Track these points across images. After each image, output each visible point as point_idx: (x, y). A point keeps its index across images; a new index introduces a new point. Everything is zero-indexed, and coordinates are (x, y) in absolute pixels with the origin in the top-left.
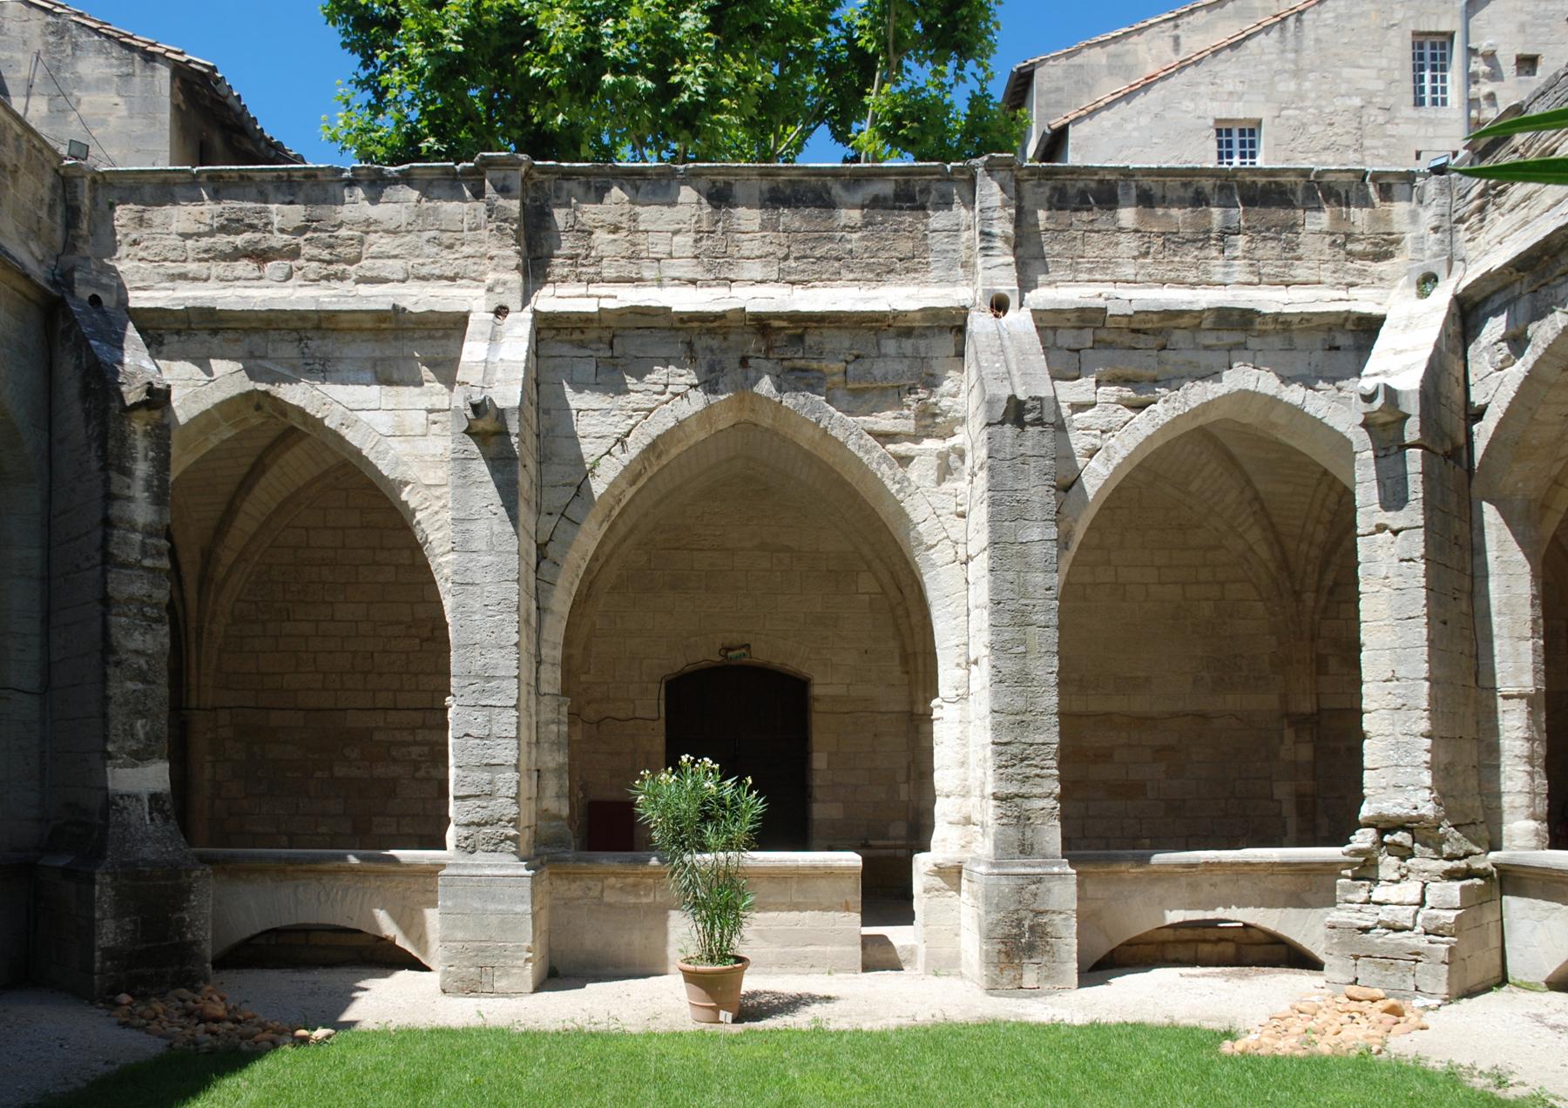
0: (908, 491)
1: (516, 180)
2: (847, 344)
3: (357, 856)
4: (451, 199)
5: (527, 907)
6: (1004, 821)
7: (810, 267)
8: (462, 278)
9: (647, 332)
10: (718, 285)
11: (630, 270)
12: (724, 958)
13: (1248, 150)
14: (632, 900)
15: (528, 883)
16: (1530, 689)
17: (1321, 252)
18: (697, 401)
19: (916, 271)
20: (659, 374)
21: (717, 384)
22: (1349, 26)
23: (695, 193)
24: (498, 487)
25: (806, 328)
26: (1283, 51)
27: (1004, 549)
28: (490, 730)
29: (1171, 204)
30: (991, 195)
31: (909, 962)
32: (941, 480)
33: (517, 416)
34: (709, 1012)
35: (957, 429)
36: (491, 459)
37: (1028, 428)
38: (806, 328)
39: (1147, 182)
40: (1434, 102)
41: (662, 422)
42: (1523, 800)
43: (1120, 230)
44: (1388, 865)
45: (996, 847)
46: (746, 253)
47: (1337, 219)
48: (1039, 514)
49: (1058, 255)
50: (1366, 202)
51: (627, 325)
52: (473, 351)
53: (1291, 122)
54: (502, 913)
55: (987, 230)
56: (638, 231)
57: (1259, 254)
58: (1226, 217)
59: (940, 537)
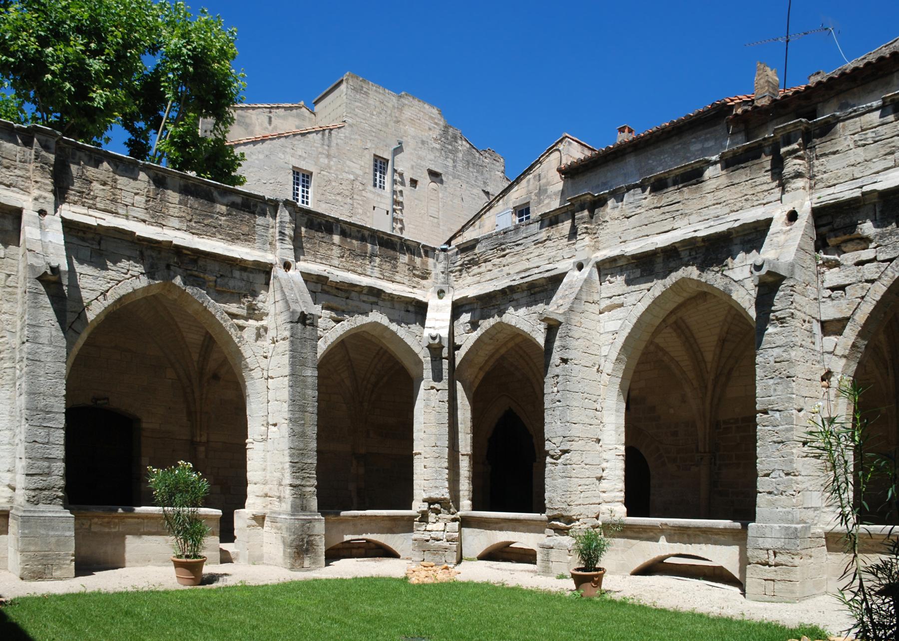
0: (243, 342)
1: (52, 143)
2: (217, 269)
3: (123, 509)
4: (10, 141)
5: (73, 533)
7: (201, 228)
8: (14, 187)
9: (119, 241)
10: (157, 226)
12: (196, 556)
13: (306, 184)
14: (107, 530)
15: (73, 520)
16: (470, 453)
17: (405, 272)
18: (144, 282)
19: (249, 241)
20: (124, 264)
23: (147, 177)
24: (55, 311)
25: (199, 257)
29: (353, 238)
31: (235, 559)
32: (257, 340)
33: (67, 276)
35: (264, 318)
39: (344, 226)
40: (380, 187)
41: (125, 288)
42: (467, 493)
43: (333, 244)
44: (432, 517)
45: (292, 507)
46: (172, 214)
47: (410, 260)
48: (310, 365)
49: (309, 249)
50: (420, 256)
52: (29, 231)
53: (325, 178)
54: (58, 536)
57: (384, 267)
58: (373, 249)
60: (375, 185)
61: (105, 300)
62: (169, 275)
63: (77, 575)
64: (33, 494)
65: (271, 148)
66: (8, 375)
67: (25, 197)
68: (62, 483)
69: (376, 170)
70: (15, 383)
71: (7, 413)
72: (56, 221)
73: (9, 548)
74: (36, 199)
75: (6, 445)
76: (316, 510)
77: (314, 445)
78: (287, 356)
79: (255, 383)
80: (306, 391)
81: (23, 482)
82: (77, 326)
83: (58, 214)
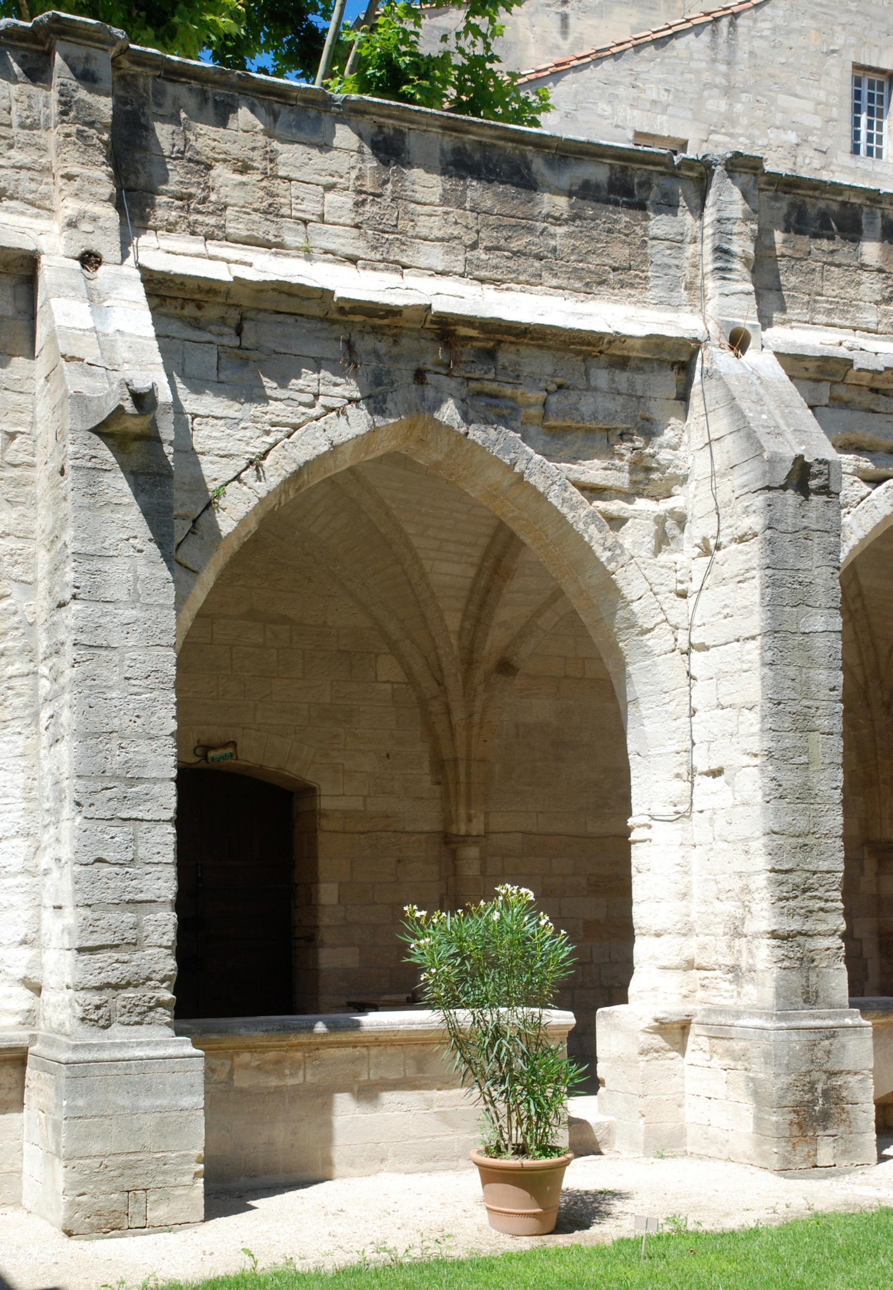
0: (622, 560)
2: (549, 369)
5: (199, 1100)
6: (786, 964)
7: (504, 263)
8: (11, 198)
9: (290, 320)
11: (265, 229)
14: (273, 1082)
15: (199, 1065)
19: (632, 286)
20: (308, 380)
21: (385, 401)
22: (787, 43)
23: (355, 138)
24: (146, 513)
25: (500, 342)
26: (714, 61)
27: (785, 639)
28: (135, 853)
30: (731, 203)
34: (532, 1221)
35: (676, 489)
36: (132, 473)
37: (813, 497)
38: (500, 342)
40: (870, 152)
43: (863, 267)
45: (778, 995)
46: (424, 232)
48: (823, 600)
49: (794, 288)
51: (262, 306)
55: (725, 246)
56: (277, 177)
59: (658, 620)
60: (856, 150)
61: (259, 479)
62: (423, 398)
63: (211, 1212)
64: (96, 999)
65: (576, 95)
66: (19, 695)
67: (41, 224)
68: (169, 965)
69: (857, 109)
70: (36, 715)
71: (18, 793)
72: (127, 278)
73: (26, 1146)
74: (72, 224)
75: (15, 875)
76: (846, 1000)
77: (835, 820)
78: (756, 582)
79: (655, 664)
80: (812, 673)
81: (67, 970)
82: (189, 554)
83: (130, 260)
